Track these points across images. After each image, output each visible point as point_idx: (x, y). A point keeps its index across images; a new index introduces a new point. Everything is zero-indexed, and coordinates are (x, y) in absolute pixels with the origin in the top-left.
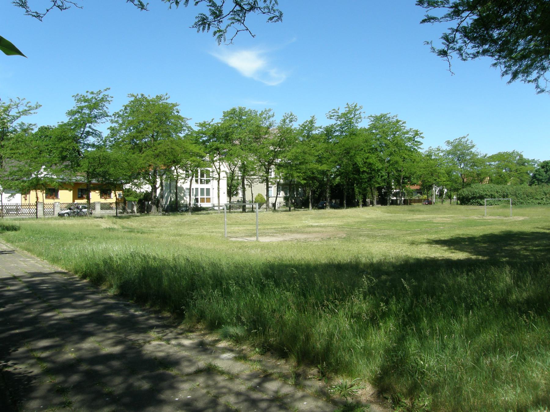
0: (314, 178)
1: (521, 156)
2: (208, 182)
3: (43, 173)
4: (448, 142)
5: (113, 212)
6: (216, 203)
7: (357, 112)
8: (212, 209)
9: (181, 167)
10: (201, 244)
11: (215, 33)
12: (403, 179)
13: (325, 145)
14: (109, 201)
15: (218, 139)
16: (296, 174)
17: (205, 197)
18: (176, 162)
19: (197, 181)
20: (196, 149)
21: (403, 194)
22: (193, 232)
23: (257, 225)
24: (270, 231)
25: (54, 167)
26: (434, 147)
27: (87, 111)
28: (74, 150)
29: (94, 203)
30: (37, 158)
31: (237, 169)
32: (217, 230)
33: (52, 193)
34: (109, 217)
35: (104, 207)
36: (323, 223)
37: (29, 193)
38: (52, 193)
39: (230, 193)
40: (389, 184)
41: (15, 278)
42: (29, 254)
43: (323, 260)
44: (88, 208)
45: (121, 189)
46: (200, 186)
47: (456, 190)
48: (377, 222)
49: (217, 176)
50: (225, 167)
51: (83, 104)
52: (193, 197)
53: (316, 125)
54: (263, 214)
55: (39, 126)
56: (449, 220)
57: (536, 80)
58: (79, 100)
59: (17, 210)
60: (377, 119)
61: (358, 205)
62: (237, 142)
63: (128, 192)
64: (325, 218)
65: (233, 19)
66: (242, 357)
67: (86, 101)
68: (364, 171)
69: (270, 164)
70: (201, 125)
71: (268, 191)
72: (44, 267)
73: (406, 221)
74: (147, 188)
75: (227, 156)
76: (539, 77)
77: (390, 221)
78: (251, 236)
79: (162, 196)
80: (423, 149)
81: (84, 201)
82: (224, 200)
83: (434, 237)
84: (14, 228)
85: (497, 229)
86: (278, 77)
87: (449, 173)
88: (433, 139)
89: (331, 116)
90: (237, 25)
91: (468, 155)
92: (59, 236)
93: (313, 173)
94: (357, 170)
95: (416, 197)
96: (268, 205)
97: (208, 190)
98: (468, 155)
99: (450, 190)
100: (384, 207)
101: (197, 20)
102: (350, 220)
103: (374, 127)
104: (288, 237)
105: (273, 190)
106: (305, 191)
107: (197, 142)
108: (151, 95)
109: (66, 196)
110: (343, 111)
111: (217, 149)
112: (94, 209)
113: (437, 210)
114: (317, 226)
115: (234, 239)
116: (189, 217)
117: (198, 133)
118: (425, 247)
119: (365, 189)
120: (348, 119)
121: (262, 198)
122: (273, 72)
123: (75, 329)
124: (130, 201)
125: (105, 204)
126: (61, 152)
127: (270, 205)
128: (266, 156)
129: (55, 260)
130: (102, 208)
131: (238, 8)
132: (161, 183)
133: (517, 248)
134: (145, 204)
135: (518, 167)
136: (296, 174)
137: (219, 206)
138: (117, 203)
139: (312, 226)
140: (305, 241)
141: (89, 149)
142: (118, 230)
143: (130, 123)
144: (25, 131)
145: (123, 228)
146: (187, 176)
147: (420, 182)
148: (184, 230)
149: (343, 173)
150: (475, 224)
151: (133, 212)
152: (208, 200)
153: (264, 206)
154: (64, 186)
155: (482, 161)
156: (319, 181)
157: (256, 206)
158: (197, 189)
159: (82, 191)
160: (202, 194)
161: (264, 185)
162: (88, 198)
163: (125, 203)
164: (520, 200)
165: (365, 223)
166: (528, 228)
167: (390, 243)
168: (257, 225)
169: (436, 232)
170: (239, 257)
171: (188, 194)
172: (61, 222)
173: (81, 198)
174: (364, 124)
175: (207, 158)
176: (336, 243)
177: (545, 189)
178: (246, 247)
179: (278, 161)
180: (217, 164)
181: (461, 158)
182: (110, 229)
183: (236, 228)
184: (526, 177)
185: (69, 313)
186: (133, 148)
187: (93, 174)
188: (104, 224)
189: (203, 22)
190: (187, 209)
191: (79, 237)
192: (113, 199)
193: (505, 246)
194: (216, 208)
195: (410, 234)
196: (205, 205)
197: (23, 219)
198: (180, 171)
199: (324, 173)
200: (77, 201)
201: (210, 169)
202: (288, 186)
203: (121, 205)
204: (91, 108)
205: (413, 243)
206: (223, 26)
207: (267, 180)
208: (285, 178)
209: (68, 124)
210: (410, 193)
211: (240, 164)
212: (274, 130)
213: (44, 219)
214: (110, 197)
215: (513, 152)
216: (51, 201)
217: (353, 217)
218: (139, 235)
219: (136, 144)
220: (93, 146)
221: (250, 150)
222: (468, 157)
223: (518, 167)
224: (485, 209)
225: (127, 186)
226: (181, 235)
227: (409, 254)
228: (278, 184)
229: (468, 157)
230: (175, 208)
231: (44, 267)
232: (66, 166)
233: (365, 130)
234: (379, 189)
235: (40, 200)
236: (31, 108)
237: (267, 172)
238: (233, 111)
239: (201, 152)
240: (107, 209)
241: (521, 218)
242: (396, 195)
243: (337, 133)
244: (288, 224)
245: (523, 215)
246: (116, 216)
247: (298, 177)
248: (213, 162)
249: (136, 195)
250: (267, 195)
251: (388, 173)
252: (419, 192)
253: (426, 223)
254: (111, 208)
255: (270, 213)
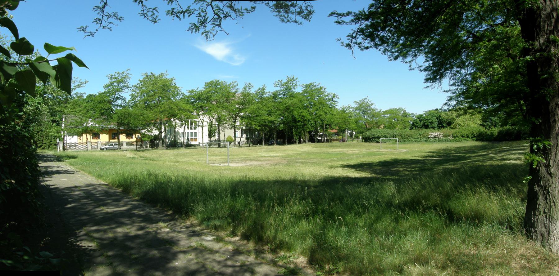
0: (265, 126)
1: (405, 111)
2: (195, 128)
3: (90, 123)
4: (356, 102)
5: (135, 147)
6: (201, 142)
7: (294, 82)
8: (198, 145)
9: (178, 119)
10: (191, 168)
11: (203, 33)
12: (326, 125)
13: (273, 104)
14: (131, 140)
15: (202, 101)
16: (253, 123)
17: (194, 138)
18: (174, 116)
19: (188, 128)
20: (187, 107)
21: (326, 136)
22: (187, 160)
23: (228, 156)
24: (236, 160)
25: (97, 120)
26: (346, 105)
27: (115, 84)
28: (108, 109)
29: (122, 142)
30: (86, 115)
31: (214, 120)
32: (202, 159)
33: (96, 135)
34: (131, 150)
35: (129, 144)
36: (271, 154)
37: (82, 135)
38: (96, 135)
39: (210, 135)
40: (316, 129)
41: (76, 187)
42: (83, 173)
43: (272, 178)
44: (119, 145)
45: (140, 133)
46: (190, 131)
47: (362, 133)
48: (308, 153)
49: (201, 125)
50: (206, 119)
51: (114, 80)
52: (186, 138)
53: (266, 91)
54: (232, 149)
55: (87, 94)
56: (357, 152)
57: (410, 62)
58: (111, 78)
59: (75, 146)
60: (308, 86)
61: (296, 143)
62: (214, 103)
63: (144, 135)
64: (273, 151)
65: (214, 24)
66: (219, 240)
67: (115, 78)
68: (299, 121)
69: (236, 116)
70: (190, 92)
71: (235, 134)
72: (92, 181)
73: (328, 153)
74: (156, 132)
75: (208, 112)
76: (412, 60)
77: (317, 153)
78: (224, 163)
79: (165, 136)
80: (339, 106)
81: (116, 140)
82: (206, 139)
83: (346, 163)
84: (74, 157)
85: (388, 158)
86: (239, 60)
87: (356, 122)
88: (346, 99)
89: (276, 85)
90: (217, 28)
91: (369, 110)
92: (100, 162)
93: (265, 122)
94: (295, 120)
95: (334, 137)
96: (235, 143)
97: (196, 133)
98: (369, 110)
99: (357, 133)
100: (313, 144)
101: (190, 26)
102: (290, 153)
103: (305, 92)
104: (249, 163)
105: (238, 133)
106: (259, 134)
107: (188, 102)
108: (157, 74)
109: (104, 137)
110: (284, 81)
111: (201, 107)
112: (122, 145)
113: (349, 146)
114: (268, 156)
115: (213, 165)
116: (183, 150)
117: (189, 97)
118: (340, 169)
119: (300, 133)
120: (288, 87)
121: (231, 138)
122: (236, 57)
123: (114, 219)
124: (145, 141)
125: (129, 142)
126: (101, 110)
127: (237, 143)
128: (233, 111)
129: (99, 176)
130: (127, 145)
131: (216, 16)
132: (165, 129)
133: (401, 169)
134: (154, 142)
135: (403, 118)
136: (253, 123)
137: (203, 144)
138: (136, 142)
139: (264, 156)
140: (260, 166)
141: (118, 108)
142: (137, 158)
143: (144, 91)
144: (79, 97)
145: (141, 157)
146: (182, 124)
147: (337, 128)
148: (180, 159)
149: (287, 121)
150: (374, 154)
151: (147, 147)
152: (196, 140)
153: (233, 143)
154: (103, 131)
155: (379, 114)
156: (269, 128)
157: (228, 143)
158: (188, 133)
159: (114, 134)
160: (192, 136)
161: (233, 131)
162: (119, 139)
163: (142, 142)
164: (403, 139)
165: (300, 154)
166: (409, 157)
167: (317, 168)
168: (228, 156)
169: (348, 160)
170: (215, 176)
171: (182, 136)
172: (102, 153)
173: (114, 138)
174: (299, 90)
175: (195, 113)
176: (280, 167)
177: (420, 132)
178: (221, 169)
179: (242, 114)
180: (201, 117)
181: (365, 112)
182: (133, 158)
183: (214, 158)
184: (407, 124)
185: (111, 209)
186: (146, 107)
187: (121, 124)
188: (129, 155)
189: (196, 28)
190: (182, 145)
191: (114, 162)
192: (134, 139)
193: (393, 168)
194: (201, 145)
195: (330, 162)
196: (193, 143)
197: (79, 152)
198: (177, 121)
199: (272, 122)
200: (111, 141)
201: (197, 120)
202: (248, 131)
203: (139, 143)
204: (120, 82)
205: (332, 167)
206: (207, 29)
207: (234, 127)
208: (247, 126)
209: (105, 93)
210: (331, 135)
211: (216, 116)
212: (238, 94)
213: (92, 152)
214: (132, 138)
215: (400, 109)
216: (93, 141)
217: (293, 151)
218: (151, 161)
219: (148, 105)
220: (121, 106)
221: (223, 107)
222: (369, 112)
223: (403, 118)
224: (380, 145)
225: (143, 131)
226: (178, 162)
227: (330, 174)
228: (242, 129)
229: (369, 112)
230: (174, 145)
231: (92, 181)
232: (104, 119)
233: (300, 94)
234: (310, 132)
235: (89, 140)
236: (82, 83)
237: (235, 122)
238: (211, 83)
239: (191, 109)
240: (130, 145)
241: (405, 151)
242: (321, 136)
243: (281, 96)
244: (249, 155)
245: (405, 148)
246: (136, 150)
247: (255, 125)
248: (199, 115)
249: (149, 137)
250: (235, 136)
251: (316, 122)
252: (337, 134)
253: (341, 154)
254: (133, 145)
255: (236, 148)
